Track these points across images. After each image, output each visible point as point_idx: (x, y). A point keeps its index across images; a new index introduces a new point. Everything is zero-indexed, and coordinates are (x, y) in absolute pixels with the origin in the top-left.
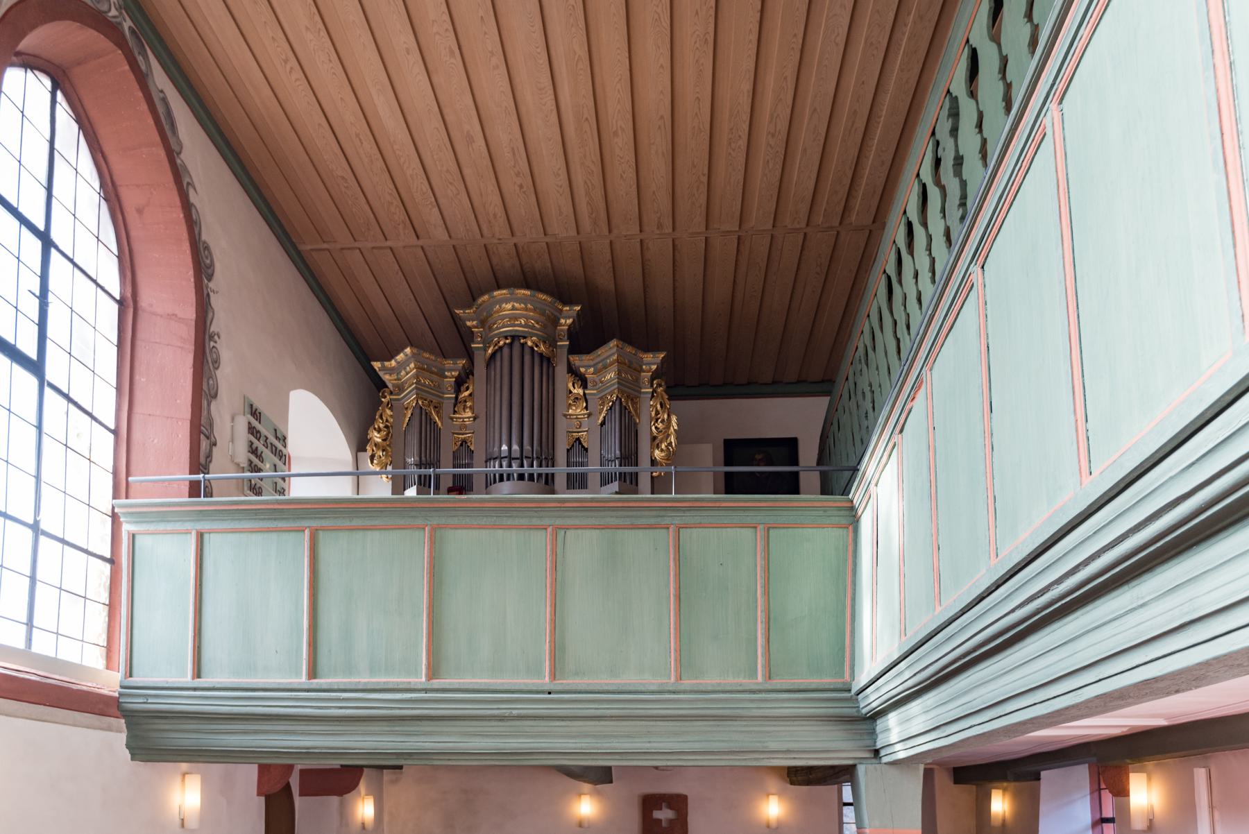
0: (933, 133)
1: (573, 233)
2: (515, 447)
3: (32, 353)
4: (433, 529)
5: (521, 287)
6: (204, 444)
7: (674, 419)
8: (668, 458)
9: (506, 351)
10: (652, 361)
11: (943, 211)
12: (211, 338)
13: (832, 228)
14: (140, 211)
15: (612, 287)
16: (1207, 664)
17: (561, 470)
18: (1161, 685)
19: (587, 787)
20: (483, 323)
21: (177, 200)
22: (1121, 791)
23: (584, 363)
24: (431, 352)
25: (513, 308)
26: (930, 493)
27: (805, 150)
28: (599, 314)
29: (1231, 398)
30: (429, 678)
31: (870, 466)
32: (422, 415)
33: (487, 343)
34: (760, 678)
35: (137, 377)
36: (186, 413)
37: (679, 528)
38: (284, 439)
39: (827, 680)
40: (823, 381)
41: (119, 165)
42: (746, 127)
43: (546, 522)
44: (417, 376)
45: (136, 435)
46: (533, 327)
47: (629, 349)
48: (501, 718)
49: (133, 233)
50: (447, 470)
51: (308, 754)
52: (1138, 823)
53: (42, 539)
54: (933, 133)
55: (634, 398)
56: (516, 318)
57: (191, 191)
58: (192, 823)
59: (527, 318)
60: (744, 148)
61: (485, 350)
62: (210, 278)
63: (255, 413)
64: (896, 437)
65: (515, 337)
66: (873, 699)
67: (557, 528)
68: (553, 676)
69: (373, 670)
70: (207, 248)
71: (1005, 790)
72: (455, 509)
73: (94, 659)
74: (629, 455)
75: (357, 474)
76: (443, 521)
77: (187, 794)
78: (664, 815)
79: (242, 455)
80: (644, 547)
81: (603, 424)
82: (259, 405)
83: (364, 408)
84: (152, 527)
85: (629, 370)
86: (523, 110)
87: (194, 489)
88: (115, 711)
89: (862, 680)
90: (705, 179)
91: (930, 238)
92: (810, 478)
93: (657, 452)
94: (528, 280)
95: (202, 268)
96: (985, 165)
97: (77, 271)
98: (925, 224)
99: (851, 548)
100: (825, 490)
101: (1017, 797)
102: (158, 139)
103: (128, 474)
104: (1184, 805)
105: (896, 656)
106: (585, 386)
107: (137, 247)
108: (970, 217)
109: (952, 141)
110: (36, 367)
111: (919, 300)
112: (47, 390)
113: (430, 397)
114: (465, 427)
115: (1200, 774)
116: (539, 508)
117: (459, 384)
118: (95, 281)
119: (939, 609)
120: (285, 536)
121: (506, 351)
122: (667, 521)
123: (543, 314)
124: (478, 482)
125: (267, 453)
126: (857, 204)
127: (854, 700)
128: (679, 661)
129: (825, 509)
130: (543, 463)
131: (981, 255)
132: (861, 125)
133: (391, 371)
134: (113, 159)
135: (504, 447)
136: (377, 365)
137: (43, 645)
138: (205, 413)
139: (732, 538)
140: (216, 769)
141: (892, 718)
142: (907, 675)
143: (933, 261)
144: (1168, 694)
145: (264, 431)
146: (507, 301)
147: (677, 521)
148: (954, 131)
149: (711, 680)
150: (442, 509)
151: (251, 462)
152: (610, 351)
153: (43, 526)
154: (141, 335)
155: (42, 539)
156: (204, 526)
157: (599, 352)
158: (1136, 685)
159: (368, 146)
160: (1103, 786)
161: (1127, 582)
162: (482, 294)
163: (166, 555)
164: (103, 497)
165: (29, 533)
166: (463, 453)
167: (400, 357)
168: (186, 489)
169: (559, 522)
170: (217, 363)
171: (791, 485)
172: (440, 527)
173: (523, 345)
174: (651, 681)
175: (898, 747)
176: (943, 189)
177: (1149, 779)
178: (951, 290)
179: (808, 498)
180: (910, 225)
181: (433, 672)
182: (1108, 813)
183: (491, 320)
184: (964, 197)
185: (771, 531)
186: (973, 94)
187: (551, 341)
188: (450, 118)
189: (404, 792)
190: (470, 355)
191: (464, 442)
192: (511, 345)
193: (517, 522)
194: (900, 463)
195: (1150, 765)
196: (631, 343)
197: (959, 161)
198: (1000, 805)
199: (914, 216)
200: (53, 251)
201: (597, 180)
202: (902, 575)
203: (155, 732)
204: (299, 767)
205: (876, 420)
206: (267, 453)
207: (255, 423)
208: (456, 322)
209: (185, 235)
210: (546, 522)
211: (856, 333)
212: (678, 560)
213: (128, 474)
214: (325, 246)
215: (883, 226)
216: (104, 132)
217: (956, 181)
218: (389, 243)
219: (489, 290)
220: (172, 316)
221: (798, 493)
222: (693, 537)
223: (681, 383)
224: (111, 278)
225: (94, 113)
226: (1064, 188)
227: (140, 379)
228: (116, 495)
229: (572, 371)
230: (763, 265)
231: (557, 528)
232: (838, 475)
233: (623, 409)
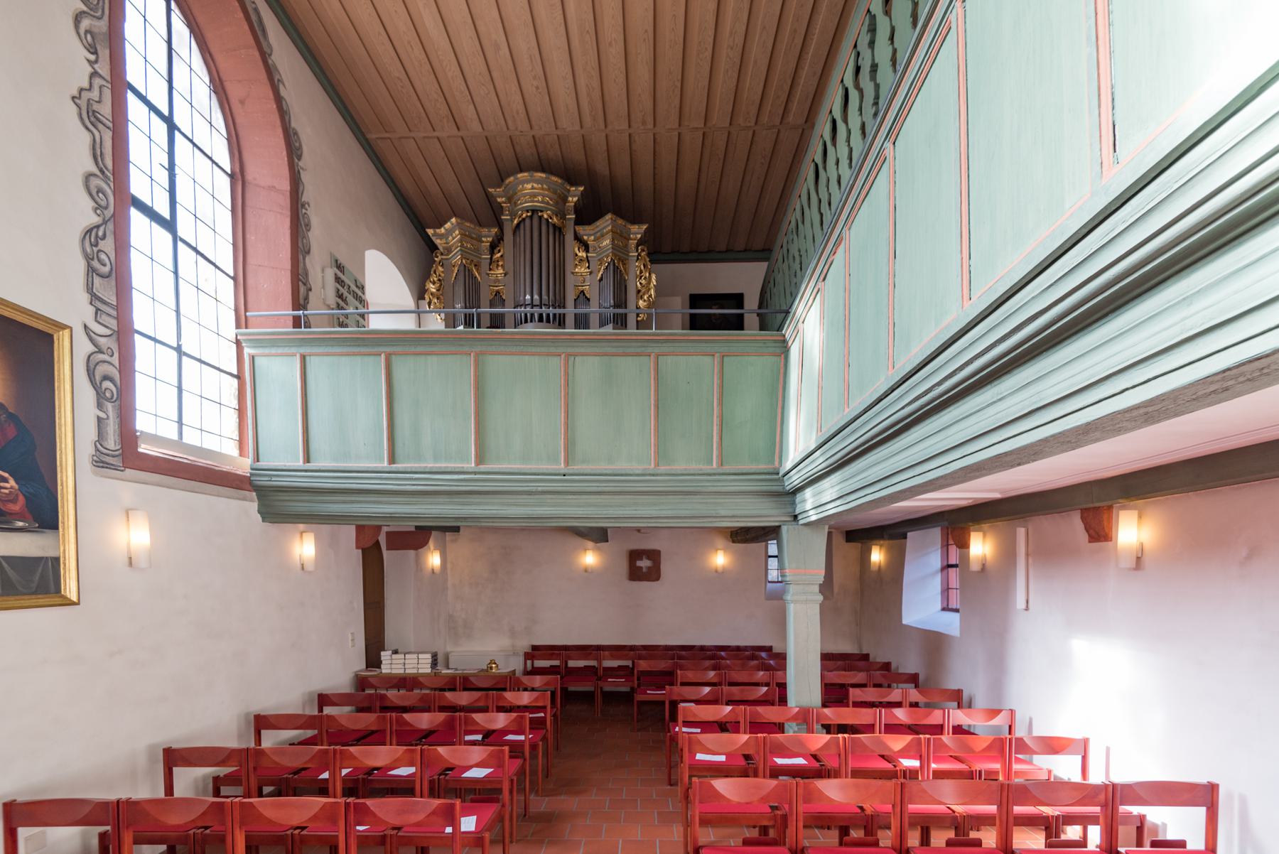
0: (855, 46)
1: (577, 127)
2: (536, 297)
3: (165, 212)
4: (477, 354)
5: (537, 171)
6: (302, 289)
7: (654, 277)
8: (649, 307)
9: (528, 221)
10: (637, 231)
11: (860, 109)
12: (303, 206)
13: (774, 126)
14: (242, 102)
15: (607, 173)
16: (1045, 441)
17: (570, 311)
18: (1008, 459)
19: (590, 544)
20: (509, 200)
21: (271, 95)
22: (964, 545)
23: (586, 232)
24: (471, 222)
25: (533, 188)
26: (843, 328)
27: (755, 62)
28: (597, 194)
29: (1086, 231)
30: (477, 464)
31: (800, 308)
32: (466, 272)
33: (513, 215)
34: (715, 465)
35: (248, 236)
36: (287, 265)
37: (658, 356)
38: (362, 288)
39: (762, 467)
40: (763, 250)
41: (222, 62)
42: (711, 40)
43: (560, 350)
44: (461, 241)
45: (250, 281)
46: (548, 203)
47: (620, 221)
48: (530, 493)
49: (238, 121)
50: (486, 310)
51: (392, 517)
52: (975, 567)
53: (184, 359)
54: (855, 46)
55: (624, 261)
56: (535, 195)
57: (281, 87)
58: (310, 567)
59: (544, 196)
60: (709, 59)
61: (512, 220)
62: (300, 158)
63: (340, 267)
64: (820, 284)
65: (534, 211)
66: (795, 479)
67: (568, 355)
68: (567, 463)
69: (436, 458)
70: (296, 133)
71: (881, 546)
72: (493, 340)
73: (231, 449)
74: (621, 302)
75: (419, 313)
76: (484, 349)
77: (305, 547)
78: (644, 564)
79: (332, 299)
80: (633, 371)
81: (601, 280)
82: (342, 260)
83: (422, 264)
84: (267, 351)
85: (620, 237)
86: (538, 21)
87: (297, 322)
88: (248, 486)
89: (788, 465)
90: (679, 85)
91: (849, 132)
92: (751, 319)
93: (641, 302)
94: (543, 165)
95: (293, 150)
96: (895, 71)
97: (196, 151)
98: (845, 121)
99: (782, 371)
100: (763, 327)
101: (890, 551)
102: (252, 42)
103: (246, 311)
104: (1007, 555)
105: (813, 447)
106: (587, 250)
107: (241, 134)
108: (882, 111)
109: (869, 51)
110: (170, 225)
111: (839, 182)
112: (180, 244)
113: (471, 257)
114: (498, 281)
115: (1021, 532)
116: (554, 340)
117: (493, 247)
118: (210, 158)
119: (847, 410)
120: (367, 359)
121: (528, 221)
122: (649, 350)
123: (555, 193)
124: (509, 320)
125: (350, 298)
126: (794, 107)
127: (781, 480)
128: (657, 453)
129: (764, 342)
130: (557, 309)
131: (893, 135)
132: (799, 41)
133: (441, 236)
134: (220, 59)
135: (528, 297)
136: (430, 232)
137: (191, 438)
138: (301, 265)
139: (696, 362)
140: (325, 529)
141: (808, 493)
142: (821, 460)
143: (851, 150)
144: (1012, 466)
145: (347, 281)
146: (528, 182)
147: (657, 350)
148: (872, 44)
149: (679, 466)
150: (483, 340)
151: (338, 305)
152: (606, 222)
153: (184, 349)
154: (248, 203)
155: (184, 359)
156: (303, 350)
157: (598, 223)
158: (990, 459)
159: (417, 52)
160: (951, 542)
161: (990, 382)
162: (509, 176)
163: (279, 371)
164: (230, 330)
165: (175, 354)
166: (498, 299)
167: (448, 225)
168: (291, 323)
169: (570, 350)
170: (308, 226)
171: (737, 323)
172: (483, 353)
173: (540, 218)
174: (637, 467)
175: (811, 513)
176: (861, 91)
177: (984, 536)
178: (866, 166)
179: (751, 331)
180: (834, 122)
181: (480, 459)
182: (953, 561)
183: (516, 197)
184: (877, 97)
185: (726, 359)
186: (887, 13)
187: (562, 214)
188: (481, 29)
189: (462, 547)
190: (500, 225)
191: (498, 292)
192: (531, 217)
193: (538, 350)
194: (822, 304)
195: (985, 526)
196: (622, 217)
197: (874, 68)
198: (877, 556)
199: (837, 114)
200: (177, 133)
201: (596, 83)
202: (820, 387)
203: (278, 501)
204: (385, 529)
205: (803, 277)
206: (350, 298)
207: (340, 274)
208: (490, 199)
209: (278, 122)
210: (560, 350)
211: (800, 180)
212: (657, 379)
213: (246, 311)
214: (387, 135)
215: (813, 126)
216: (209, 36)
217: (872, 84)
218: (436, 134)
219: (513, 173)
220: (272, 188)
221: (742, 328)
222: (668, 362)
223: (660, 250)
224: (225, 160)
225: (201, 19)
226: (892, 196)
227: (251, 238)
228: (238, 326)
229: (578, 238)
230: (722, 157)
231: (568, 355)
232: (774, 314)
233: (616, 269)
